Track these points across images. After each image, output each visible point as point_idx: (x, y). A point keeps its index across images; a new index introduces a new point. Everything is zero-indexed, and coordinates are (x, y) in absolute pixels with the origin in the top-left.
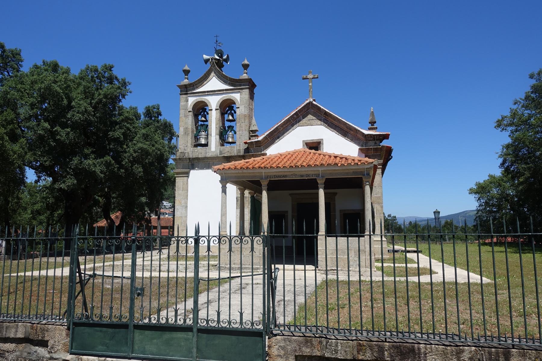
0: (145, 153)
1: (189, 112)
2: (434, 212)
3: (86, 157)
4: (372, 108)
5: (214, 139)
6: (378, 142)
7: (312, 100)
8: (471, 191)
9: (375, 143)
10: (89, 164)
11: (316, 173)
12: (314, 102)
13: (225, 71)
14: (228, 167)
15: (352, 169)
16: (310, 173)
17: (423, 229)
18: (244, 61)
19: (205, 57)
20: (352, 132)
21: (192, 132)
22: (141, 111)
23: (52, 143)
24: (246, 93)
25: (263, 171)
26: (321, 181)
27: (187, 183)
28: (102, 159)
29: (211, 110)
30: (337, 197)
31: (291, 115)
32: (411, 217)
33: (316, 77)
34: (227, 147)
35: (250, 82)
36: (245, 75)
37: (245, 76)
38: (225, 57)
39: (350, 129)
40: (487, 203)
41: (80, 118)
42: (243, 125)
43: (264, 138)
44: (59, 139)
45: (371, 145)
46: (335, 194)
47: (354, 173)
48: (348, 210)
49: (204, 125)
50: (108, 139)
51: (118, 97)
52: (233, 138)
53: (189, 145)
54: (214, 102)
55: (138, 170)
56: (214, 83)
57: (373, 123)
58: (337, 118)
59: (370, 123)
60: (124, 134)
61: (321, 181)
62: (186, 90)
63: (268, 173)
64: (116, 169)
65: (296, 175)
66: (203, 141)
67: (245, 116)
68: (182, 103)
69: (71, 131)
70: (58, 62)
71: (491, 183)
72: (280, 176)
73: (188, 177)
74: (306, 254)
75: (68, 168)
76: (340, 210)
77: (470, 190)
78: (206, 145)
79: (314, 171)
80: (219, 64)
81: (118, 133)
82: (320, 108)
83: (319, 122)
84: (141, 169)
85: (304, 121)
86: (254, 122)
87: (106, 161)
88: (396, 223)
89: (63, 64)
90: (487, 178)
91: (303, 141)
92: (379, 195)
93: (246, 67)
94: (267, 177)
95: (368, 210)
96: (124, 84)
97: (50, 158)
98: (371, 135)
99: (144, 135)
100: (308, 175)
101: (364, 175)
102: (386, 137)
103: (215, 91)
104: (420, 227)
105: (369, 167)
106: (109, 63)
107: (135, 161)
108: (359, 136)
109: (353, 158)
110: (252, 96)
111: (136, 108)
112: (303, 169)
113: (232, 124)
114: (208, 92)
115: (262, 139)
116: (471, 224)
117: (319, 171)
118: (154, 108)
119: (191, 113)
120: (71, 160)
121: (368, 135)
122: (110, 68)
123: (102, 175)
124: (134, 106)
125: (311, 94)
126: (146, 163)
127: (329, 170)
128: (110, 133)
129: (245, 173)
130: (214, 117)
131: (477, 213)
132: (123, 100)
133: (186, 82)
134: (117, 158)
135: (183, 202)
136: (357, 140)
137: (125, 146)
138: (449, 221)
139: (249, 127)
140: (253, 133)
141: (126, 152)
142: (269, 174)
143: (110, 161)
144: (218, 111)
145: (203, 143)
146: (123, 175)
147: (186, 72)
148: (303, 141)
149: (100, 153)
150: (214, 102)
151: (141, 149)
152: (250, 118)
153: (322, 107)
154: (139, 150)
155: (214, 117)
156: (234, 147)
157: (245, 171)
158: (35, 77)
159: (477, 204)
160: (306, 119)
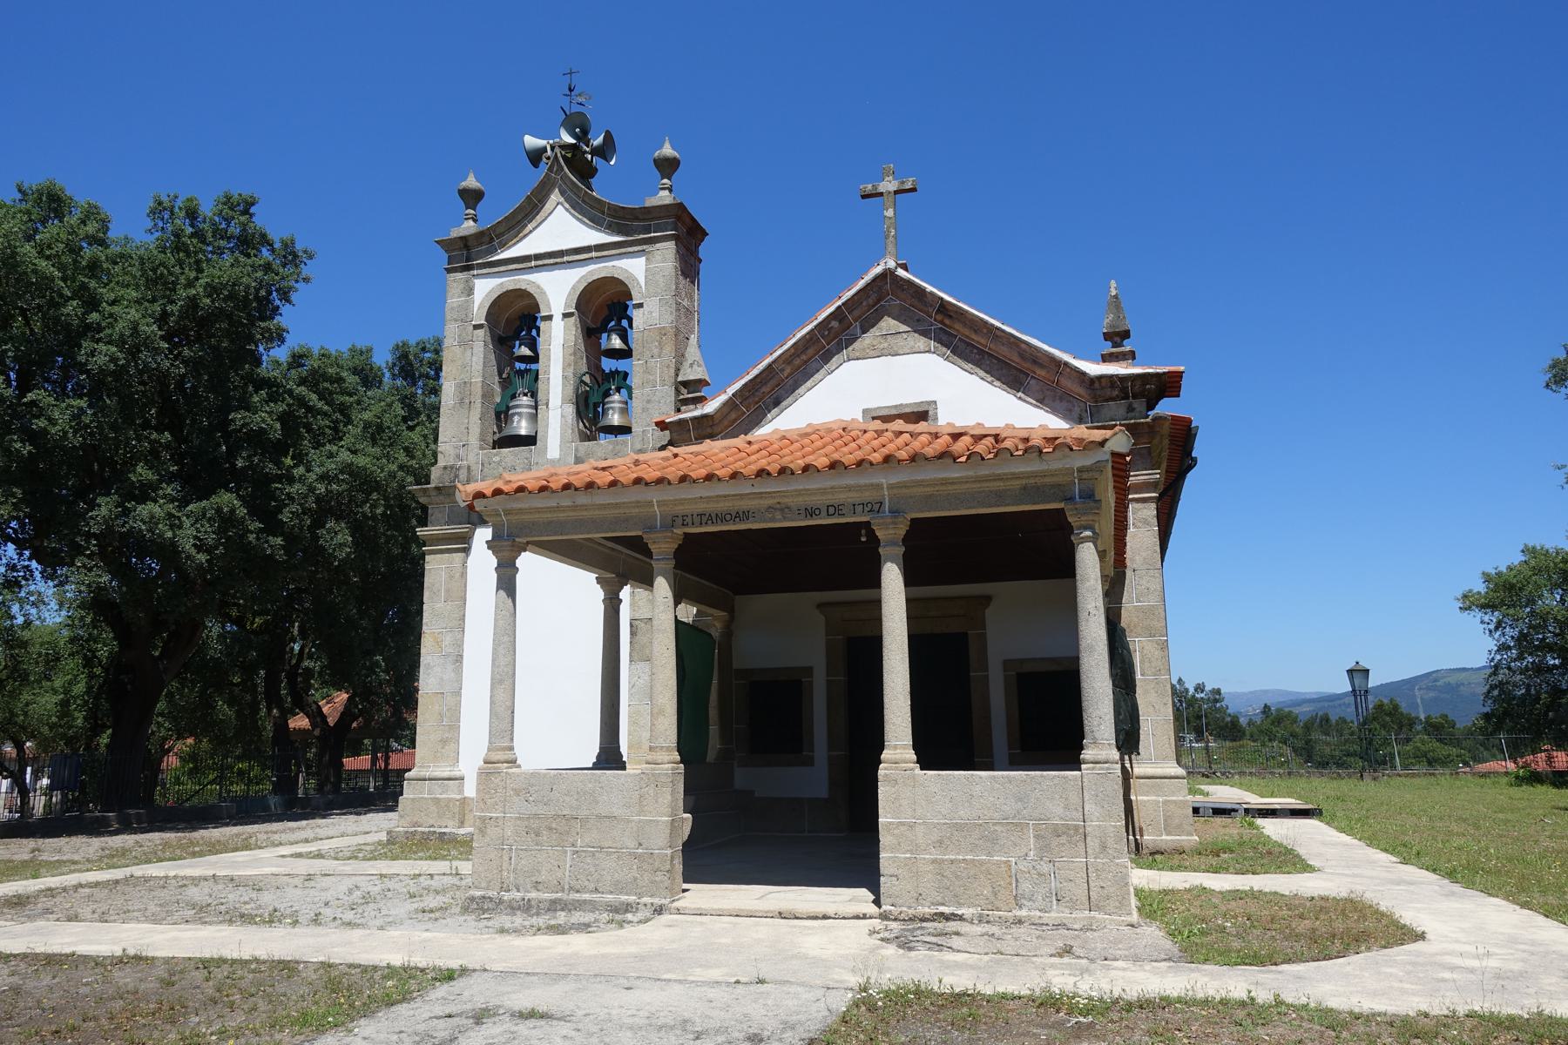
0: (364, 482)
1: (476, 327)
2: (1350, 672)
3: (144, 494)
4: (1113, 284)
6: (1139, 405)
7: (892, 264)
8: (1469, 602)
9: (1130, 409)
10: (152, 517)
11: (868, 496)
12: (901, 272)
13: (601, 189)
15: (1016, 476)
16: (841, 497)
18: (661, 147)
19: (531, 141)
20: (1041, 372)
21: (487, 395)
22: (382, 358)
23: (18, 445)
24: (665, 254)
25: (654, 495)
26: (890, 533)
27: (464, 574)
28: (204, 503)
29: (550, 318)
32: (1266, 692)
33: (908, 186)
35: (678, 218)
37: (664, 198)
38: (598, 141)
39: (1035, 362)
40: (1522, 639)
41: (113, 360)
42: (656, 364)
43: (725, 404)
44: (44, 431)
46: (987, 600)
47: (1029, 492)
48: (1034, 660)
49: (527, 371)
50: (227, 436)
51: (267, 299)
53: (474, 440)
54: (557, 291)
55: (338, 538)
56: (561, 227)
57: (1118, 336)
58: (986, 323)
59: (1107, 336)
60: (284, 418)
61: (890, 533)
62: (467, 254)
64: (252, 537)
65: (784, 510)
66: (523, 428)
67: (662, 332)
68: (454, 300)
69: (90, 406)
70: (60, 183)
71: (1537, 571)
72: (721, 518)
73: (467, 551)
74: (833, 839)
75: (79, 533)
77: (1465, 596)
78: (530, 440)
79: (859, 488)
81: (264, 417)
82: (923, 290)
83: (922, 342)
84: (344, 537)
85: (868, 339)
86: (693, 352)
87: (219, 510)
88: (1223, 710)
89: (80, 194)
90: (1517, 558)
92: (1152, 601)
93: (667, 167)
94: (671, 522)
95: (1091, 648)
96: (291, 256)
98: (1111, 377)
99: (367, 425)
101: (1071, 499)
102: (1168, 385)
103: (561, 253)
104: (1295, 721)
105: (1088, 460)
106: (239, 190)
107: (326, 509)
108: (1069, 384)
110: (689, 267)
111: (370, 350)
112: (813, 484)
113: (621, 365)
114: (538, 257)
115: (719, 410)
116: (1468, 715)
117: (879, 487)
118: (424, 349)
119: (481, 332)
120: (93, 505)
121: (1100, 378)
122: (247, 207)
123: (202, 558)
124: (361, 344)
125: (891, 248)
126: (364, 514)
127: (920, 483)
128: (238, 417)
129: (585, 507)
130: (558, 342)
131: (1495, 673)
132: (285, 309)
133: (469, 227)
134: (264, 504)
135: (448, 639)
136: (1061, 399)
137: (288, 461)
138: (1386, 701)
139: (677, 371)
140: (689, 391)
141: (291, 480)
143: (233, 511)
144: (572, 319)
145: (523, 432)
146: (281, 556)
147: (472, 198)
149: (198, 480)
150: (557, 291)
151: (348, 468)
152: (680, 339)
153: (930, 288)
154: (342, 472)
155: (558, 342)
156: (625, 443)
157: (582, 499)
158: (27, 247)
159: (1492, 644)
160: (874, 331)
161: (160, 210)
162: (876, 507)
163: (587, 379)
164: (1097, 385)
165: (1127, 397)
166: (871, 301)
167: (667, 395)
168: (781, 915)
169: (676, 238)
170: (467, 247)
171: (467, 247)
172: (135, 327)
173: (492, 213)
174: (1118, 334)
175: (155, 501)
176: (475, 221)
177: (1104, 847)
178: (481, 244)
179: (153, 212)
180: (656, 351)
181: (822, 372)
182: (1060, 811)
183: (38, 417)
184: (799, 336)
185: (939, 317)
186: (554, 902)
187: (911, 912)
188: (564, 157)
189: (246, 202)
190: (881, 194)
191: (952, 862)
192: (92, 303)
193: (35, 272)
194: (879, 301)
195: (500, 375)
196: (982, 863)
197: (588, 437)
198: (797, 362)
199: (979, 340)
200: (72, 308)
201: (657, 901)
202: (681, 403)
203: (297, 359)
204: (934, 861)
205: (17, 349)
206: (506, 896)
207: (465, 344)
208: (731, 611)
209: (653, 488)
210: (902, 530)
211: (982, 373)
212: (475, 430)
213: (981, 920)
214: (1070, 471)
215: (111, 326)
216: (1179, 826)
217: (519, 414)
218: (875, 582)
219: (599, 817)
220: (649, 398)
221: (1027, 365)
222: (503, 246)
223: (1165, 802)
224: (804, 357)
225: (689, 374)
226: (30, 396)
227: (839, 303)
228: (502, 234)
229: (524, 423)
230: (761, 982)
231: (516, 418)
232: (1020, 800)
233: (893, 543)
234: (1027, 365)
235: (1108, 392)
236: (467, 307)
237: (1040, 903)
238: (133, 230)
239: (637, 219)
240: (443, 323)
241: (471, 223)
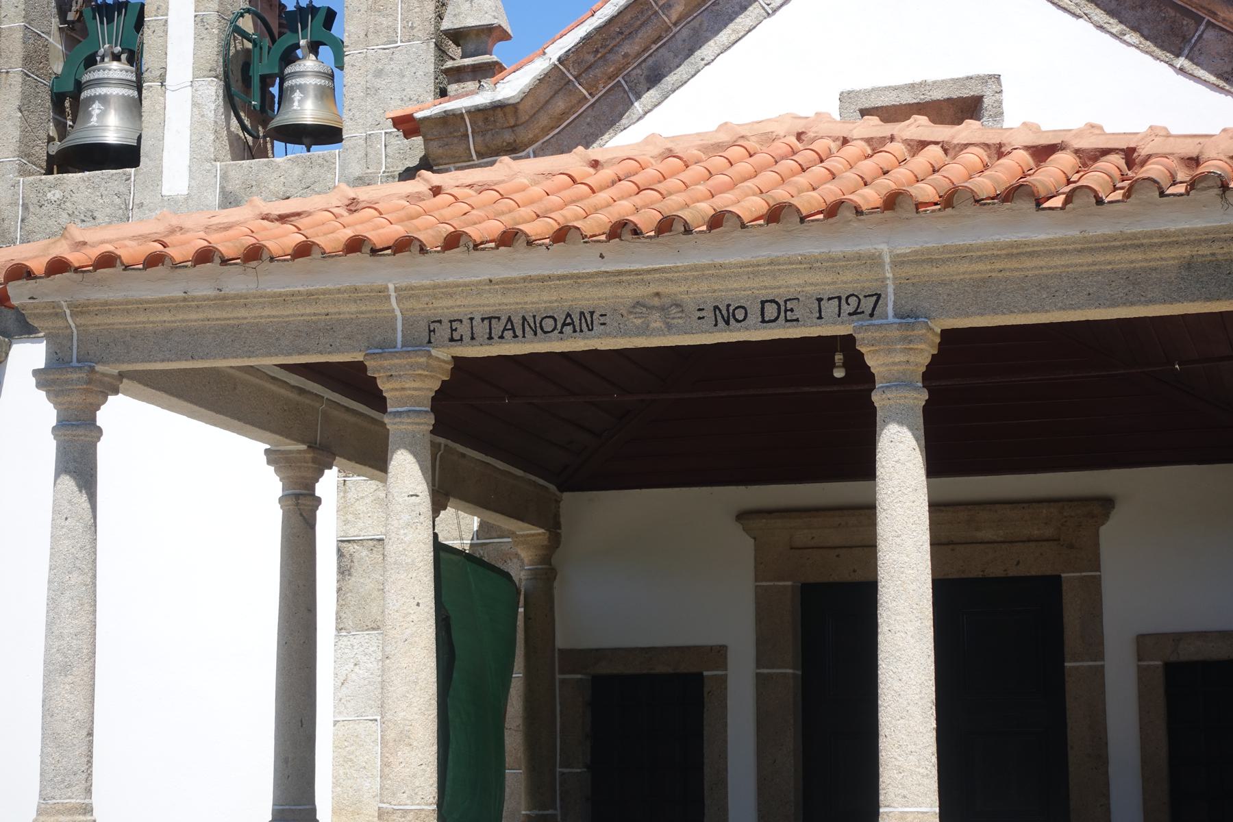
11: (849, 281)
16: (790, 284)
17: (186, 199)
21: (34, 59)
25: (390, 276)
26: (897, 365)
30: (1111, 535)
43: (543, 80)
46: (1105, 504)
48: (1202, 635)
52: (328, 93)
61: (897, 365)
63: (438, 291)
65: (670, 308)
66: (109, 127)
72: (534, 325)
76: (1141, 639)
79: (832, 264)
94: (429, 332)
100: (783, 309)
109: (1191, 149)
117: (874, 261)
129: (242, 300)
142: (445, 307)
156: (327, 163)
162: (866, 304)
163: (247, 24)
167: (420, 61)
208: (553, 525)
209: (388, 259)
210: (923, 353)
218: (861, 463)
233: (902, 383)
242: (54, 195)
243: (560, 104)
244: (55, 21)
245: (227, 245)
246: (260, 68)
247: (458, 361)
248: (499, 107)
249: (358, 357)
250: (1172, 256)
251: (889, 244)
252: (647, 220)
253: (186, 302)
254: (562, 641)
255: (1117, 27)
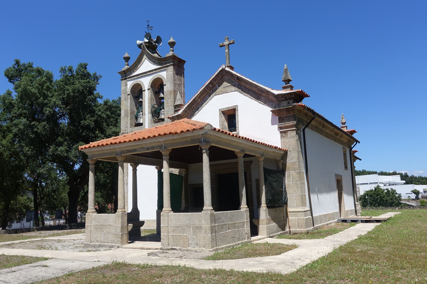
3: (60, 144)
5: (146, 118)
7: (224, 67)
9: (289, 103)
11: (159, 144)
14: (93, 145)
15: (188, 137)
16: (154, 145)
19: (139, 42)
20: (264, 95)
23: (31, 135)
29: (145, 90)
30: (252, 166)
31: (206, 85)
33: (232, 42)
34: (159, 125)
35: (174, 59)
36: (172, 52)
37: (171, 54)
42: (169, 101)
43: (183, 111)
45: (284, 105)
47: (193, 141)
53: (129, 125)
56: (147, 65)
58: (248, 81)
61: (165, 153)
62: (125, 75)
68: (123, 88)
69: (47, 123)
80: (151, 47)
83: (233, 88)
85: (220, 89)
86: (178, 96)
91: (220, 110)
93: (172, 44)
97: (31, 148)
106: (83, 62)
114: (141, 74)
117: (160, 142)
119: (129, 96)
121: (278, 95)
127: (169, 140)
129: (104, 150)
130: (147, 96)
133: (126, 67)
136: (270, 102)
142: (123, 149)
147: (127, 59)
148: (220, 110)
150: (146, 83)
155: (147, 96)
160: (222, 86)
161: (63, 70)
162: (161, 147)
163: (156, 106)
164: (278, 97)
165: (287, 100)
166: (220, 78)
167: (172, 109)
168: (141, 249)
169: (173, 65)
170: (125, 73)
171: (125, 73)
172: (55, 102)
173: (131, 62)
174: (286, 80)
175: (63, 146)
176: (128, 65)
177: (206, 232)
178: (128, 72)
179: (61, 71)
180: (169, 97)
181: (209, 99)
182: (197, 222)
183: (35, 128)
184: (201, 90)
185: (237, 81)
186: (99, 245)
187: (166, 248)
188: (146, 46)
189: (85, 65)
190: (224, 45)
191: (176, 235)
192: (45, 97)
193: (31, 92)
194: (222, 78)
195: (136, 106)
196: (182, 236)
197: (156, 122)
198: (202, 97)
199: (248, 86)
200: (41, 100)
201: (118, 245)
202: (176, 111)
203: (106, 103)
204: (172, 235)
205: (29, 111)
206: (91, 244)
207: (126, 99)
208: (187, 170)
209: (114, 145)
210: (168, 153)
211: (249, 96)
212: (129, 123)
213: (180, 250)
214: (199, 135)
215: (50, 103)
216: (302, 226)
217: (140, 117)
218: (201, 161)
219: (108, 225)
220: (168, 111)
221: (260, 93)
222: (134, 72)
223: (298, 219)
224: (203, 96)
225: (177, 103)
226: (32, 123)
227: (211, 80)
228: (133, 69)
229: (163, 116)
230: (99, 261)
231: (139, 118)
232: (189, 220)
233: (166, 156)
234: (260, 93)
235: (282, 99)
236: (126, 89)
237: (193, 246)
238: (57, 77)
239: (164, 61)
240: (121, 94)
241: (127, 66)
242: (134, 130)
243: (186, 114)
244: (135, 108)
245: (132, 140)
246: (157, 112)
247: (172, 149)
248: (179, 115)
249: (198, 144)
250: (189, 139)
251: (161, 139)
252: (137, 139)
253: (99, 151)
254: (189, 183)
255: (251, 97)
